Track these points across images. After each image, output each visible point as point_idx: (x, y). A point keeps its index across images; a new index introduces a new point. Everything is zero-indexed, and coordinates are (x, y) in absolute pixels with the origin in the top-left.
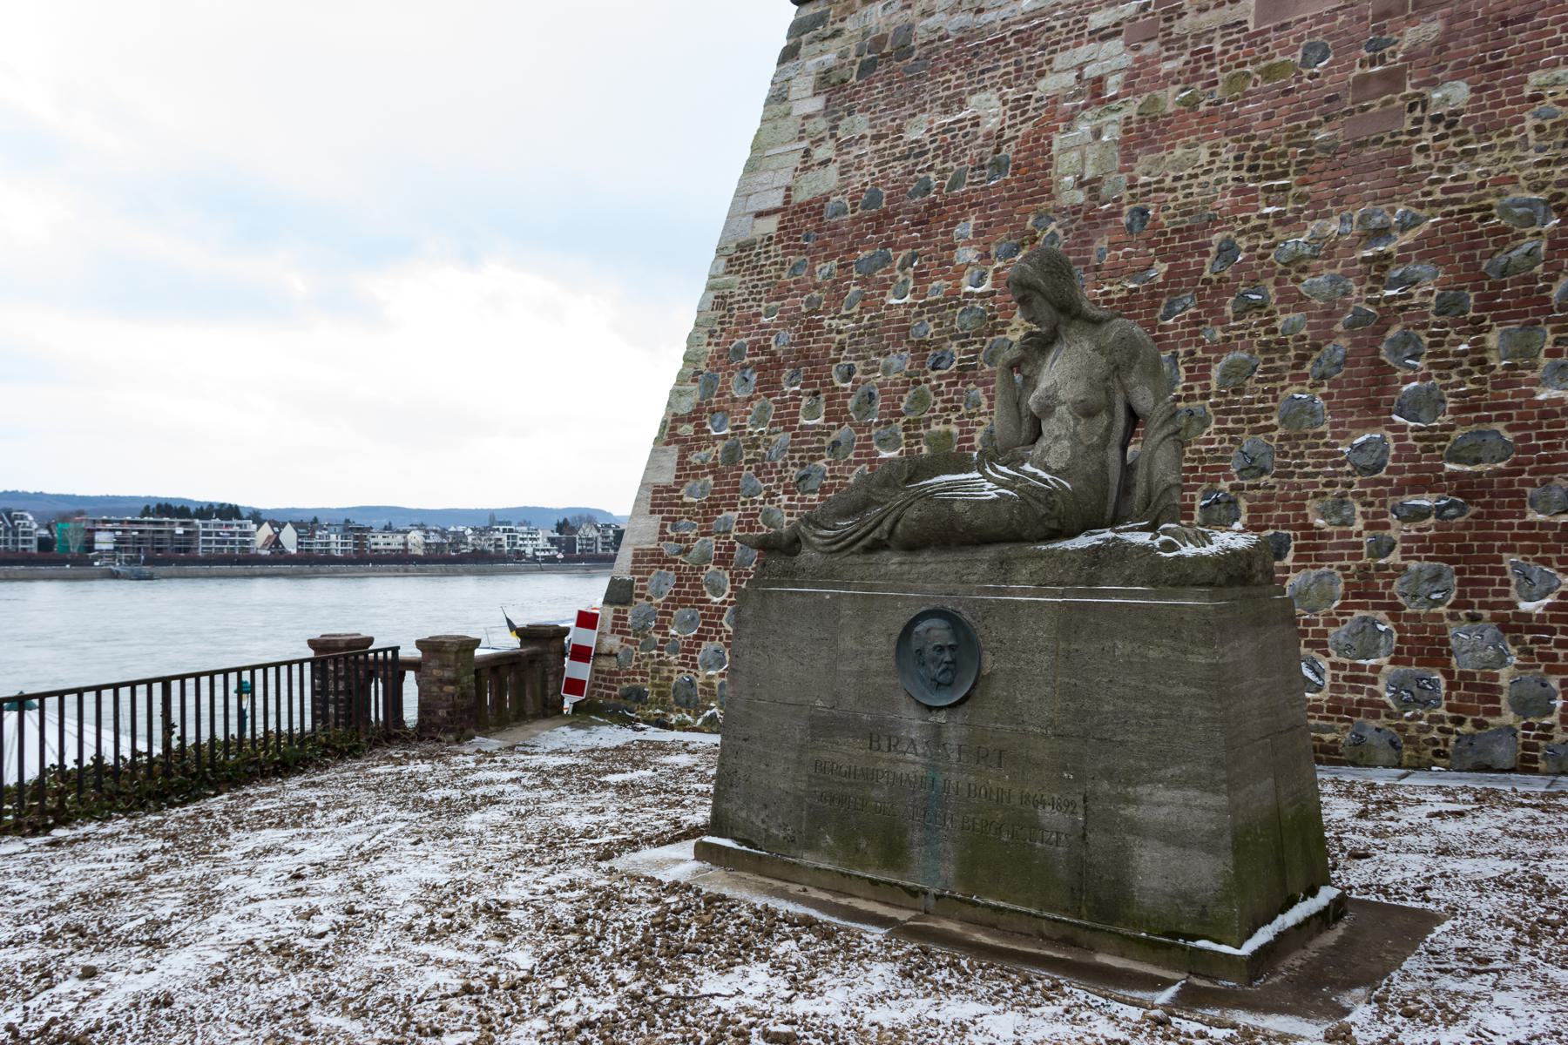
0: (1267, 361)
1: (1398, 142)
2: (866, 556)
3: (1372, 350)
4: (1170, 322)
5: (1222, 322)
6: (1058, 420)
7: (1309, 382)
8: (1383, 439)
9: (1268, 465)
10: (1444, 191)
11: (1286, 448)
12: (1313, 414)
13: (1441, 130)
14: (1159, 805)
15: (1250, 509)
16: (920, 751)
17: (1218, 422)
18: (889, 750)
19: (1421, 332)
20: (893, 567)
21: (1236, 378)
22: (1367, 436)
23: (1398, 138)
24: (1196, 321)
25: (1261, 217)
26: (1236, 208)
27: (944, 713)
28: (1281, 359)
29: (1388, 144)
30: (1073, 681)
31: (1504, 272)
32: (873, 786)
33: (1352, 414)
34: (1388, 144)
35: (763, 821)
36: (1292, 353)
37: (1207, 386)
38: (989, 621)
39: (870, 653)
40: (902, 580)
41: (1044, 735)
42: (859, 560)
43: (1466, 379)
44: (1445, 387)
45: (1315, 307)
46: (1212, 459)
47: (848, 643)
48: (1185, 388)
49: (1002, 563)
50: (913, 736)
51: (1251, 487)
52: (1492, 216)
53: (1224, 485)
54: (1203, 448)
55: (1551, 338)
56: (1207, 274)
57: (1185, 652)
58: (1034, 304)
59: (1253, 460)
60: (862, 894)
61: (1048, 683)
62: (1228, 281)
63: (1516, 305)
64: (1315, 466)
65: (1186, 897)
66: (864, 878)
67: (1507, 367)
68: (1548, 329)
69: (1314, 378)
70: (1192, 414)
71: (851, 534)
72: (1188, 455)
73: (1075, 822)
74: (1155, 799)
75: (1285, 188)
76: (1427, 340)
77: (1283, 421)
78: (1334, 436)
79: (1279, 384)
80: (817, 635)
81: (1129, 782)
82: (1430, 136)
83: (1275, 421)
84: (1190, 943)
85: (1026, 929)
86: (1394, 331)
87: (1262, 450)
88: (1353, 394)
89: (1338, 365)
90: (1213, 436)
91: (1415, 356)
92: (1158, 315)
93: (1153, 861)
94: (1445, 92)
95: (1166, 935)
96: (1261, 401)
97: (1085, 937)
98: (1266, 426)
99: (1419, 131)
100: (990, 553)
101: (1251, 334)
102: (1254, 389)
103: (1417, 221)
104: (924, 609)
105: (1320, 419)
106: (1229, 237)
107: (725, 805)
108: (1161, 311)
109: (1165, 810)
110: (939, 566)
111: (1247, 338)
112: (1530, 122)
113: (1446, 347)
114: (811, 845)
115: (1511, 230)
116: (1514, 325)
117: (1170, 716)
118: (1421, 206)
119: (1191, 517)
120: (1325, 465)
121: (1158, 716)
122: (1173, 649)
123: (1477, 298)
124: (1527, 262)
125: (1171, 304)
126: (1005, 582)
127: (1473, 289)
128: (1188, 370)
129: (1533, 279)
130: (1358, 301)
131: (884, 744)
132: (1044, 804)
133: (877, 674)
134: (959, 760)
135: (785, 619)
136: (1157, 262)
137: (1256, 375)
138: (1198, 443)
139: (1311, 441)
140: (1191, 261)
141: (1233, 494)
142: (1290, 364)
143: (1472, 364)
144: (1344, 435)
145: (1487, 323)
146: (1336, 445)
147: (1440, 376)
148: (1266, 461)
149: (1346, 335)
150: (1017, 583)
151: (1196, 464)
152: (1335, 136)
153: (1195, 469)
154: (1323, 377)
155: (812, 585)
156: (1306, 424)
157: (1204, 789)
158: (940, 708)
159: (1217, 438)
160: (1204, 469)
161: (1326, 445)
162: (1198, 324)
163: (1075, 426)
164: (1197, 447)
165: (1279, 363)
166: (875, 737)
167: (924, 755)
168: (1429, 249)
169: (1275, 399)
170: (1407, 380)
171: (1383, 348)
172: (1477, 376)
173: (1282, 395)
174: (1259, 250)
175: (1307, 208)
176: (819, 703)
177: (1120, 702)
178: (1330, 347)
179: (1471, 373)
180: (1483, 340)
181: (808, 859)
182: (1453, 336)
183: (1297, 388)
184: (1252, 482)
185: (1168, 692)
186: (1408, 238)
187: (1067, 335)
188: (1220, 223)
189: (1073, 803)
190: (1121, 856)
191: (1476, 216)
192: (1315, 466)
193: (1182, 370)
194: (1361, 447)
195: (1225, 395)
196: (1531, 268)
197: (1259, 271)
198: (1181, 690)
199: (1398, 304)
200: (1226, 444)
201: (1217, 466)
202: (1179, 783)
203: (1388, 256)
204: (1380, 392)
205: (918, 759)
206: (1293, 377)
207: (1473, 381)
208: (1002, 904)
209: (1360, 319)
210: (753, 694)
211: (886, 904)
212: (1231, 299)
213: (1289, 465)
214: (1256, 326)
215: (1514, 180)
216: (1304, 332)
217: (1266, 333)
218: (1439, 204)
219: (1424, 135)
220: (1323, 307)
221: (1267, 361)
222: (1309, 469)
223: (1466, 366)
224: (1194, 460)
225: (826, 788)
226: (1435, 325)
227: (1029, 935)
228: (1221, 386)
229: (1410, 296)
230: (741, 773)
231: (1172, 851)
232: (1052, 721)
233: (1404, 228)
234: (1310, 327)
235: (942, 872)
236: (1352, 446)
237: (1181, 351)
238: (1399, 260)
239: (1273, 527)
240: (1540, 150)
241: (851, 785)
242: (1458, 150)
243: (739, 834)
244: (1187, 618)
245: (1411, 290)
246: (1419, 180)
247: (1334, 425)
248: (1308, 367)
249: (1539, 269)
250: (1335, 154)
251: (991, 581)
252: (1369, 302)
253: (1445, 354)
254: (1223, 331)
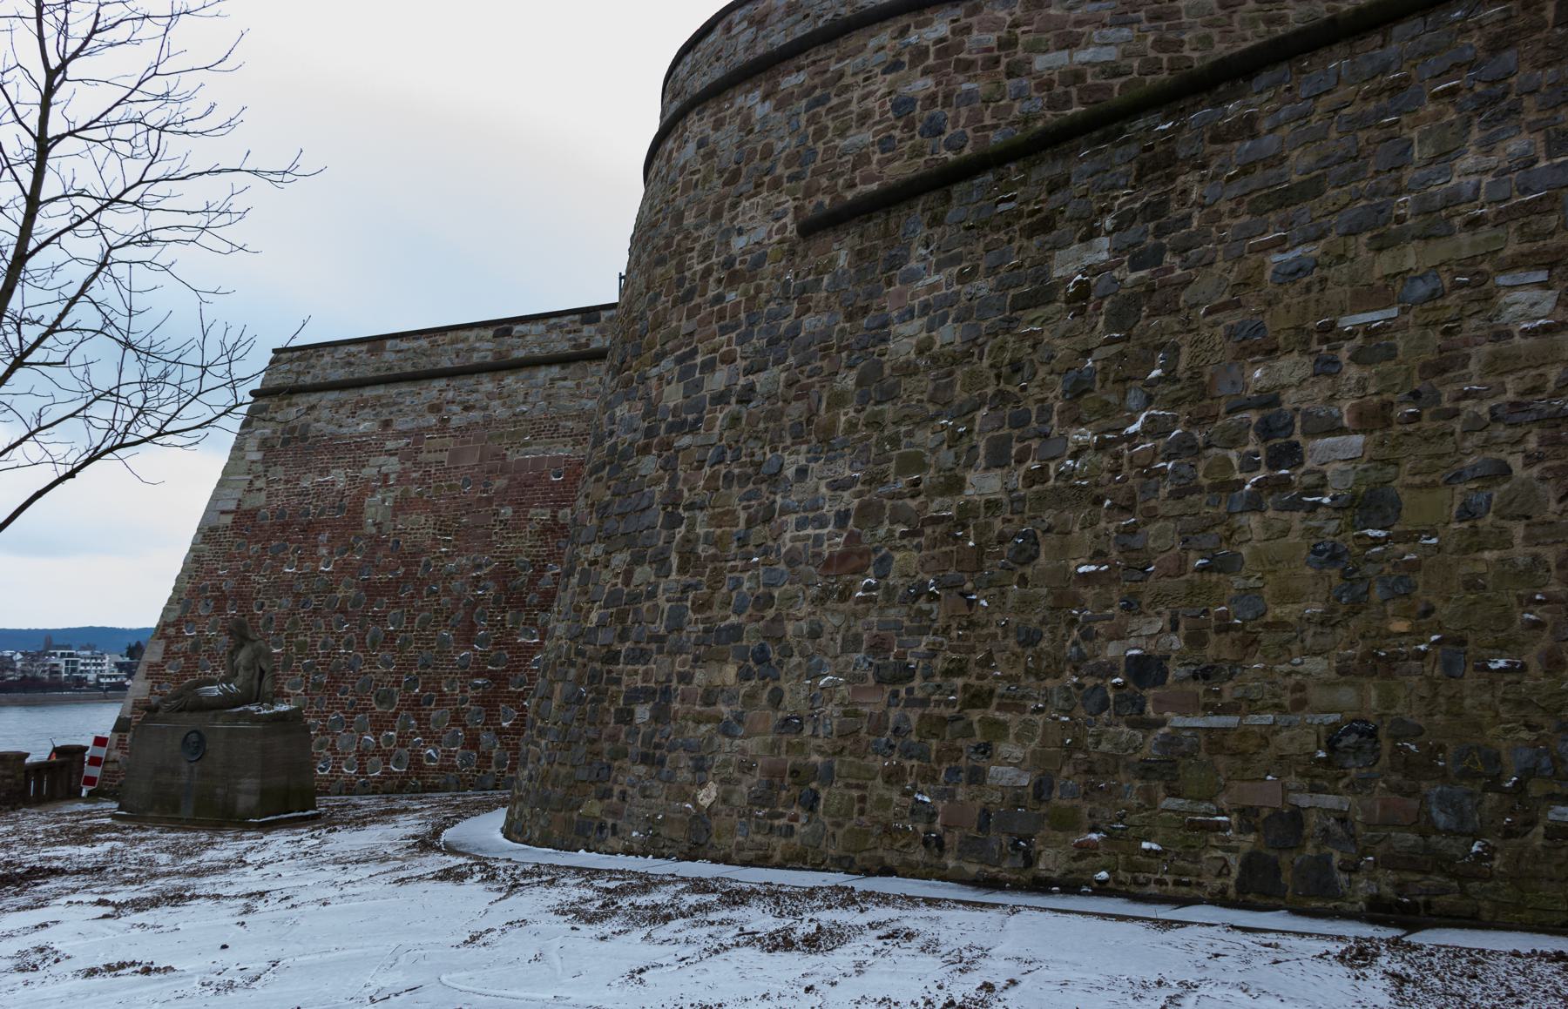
5: (422, 598)
100: (212, 713)
112: (528, 529)
148: (430, 662)
181: (150, 814)
186: (486, 570)
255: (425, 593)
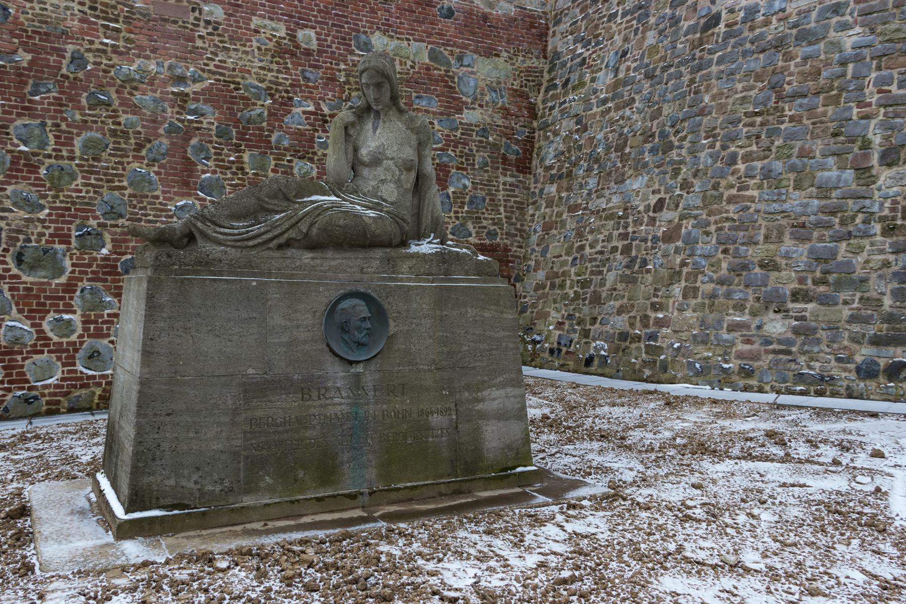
0: (115, 142)
1: (187, 28)
2: (282, 252)
3: (183, 150)
4: (37, 98)
5: (81, 109)
6: (385, 169)
7: (146, 162)
8: (194, 204)
9: (123, 213)
10: (215, 66)
11: (135, 202)
12: (150, 183)
13: (210, 30)
14: (494, 400)
15: (113, 240)
16: (344, 394)
17: (83, 178)
18: (319, 398)
19: (209, 145)
20: (307, 261)
21: (94, 149)
22: (184, 202)
23: (186, 25)
24: (58, 102)
25: (102, 43)
26: (82, 32)
27: (362, 365)
28: (125, 143)
29: (180, 26)
30: (445, 334)
31: (248, 122)
32: (306, 428)
33: (174, 187)
34: (180, 26)
35: (196, 483)
36: (133, 141)
37: (72, 151)
38: (390, 299)
39: (298, 327)
40: (316, 271)
41: (430, 370)
42: (277, 254)
43: (235, 177)
44: (225, 179)
45: (145, 114)
46: (81, 204)
47: (276, 319)
48: (54, 150)
49: (389, 260)
50: (338, 385)
51: (112, 226)
52: (240, 89)
53: (93, 223)
54: (74, 195)
55: (273, 163)
56: (64, 71)
57: (502, 312)
58: (384, 89)
59: (112, 207)
60: (310, 511)
61: (430, 337)
62: (81, 80)
63: (257, 141)
64: (154, 216)
65: (509, 447)
66: (311, 499)
67: (254, 174)
68: (272, 157)
69: (149, 160)
70: (62, 169)
71: (264, 233)
72: (62, 198)
73: (451, 420)
74: (492, 397)
75: (118, 30)
76: (213, 151)
77: (131, 184)
78: (165, 198)
79: (125, 160)
80: (244, 315)
81: (479, 390)
82: (205, 31)
83: (125, 183)
84: (513, 471)
85: (432, 494)
86: (194, 141)
87: (118, 202)
88: (174, 175)
89: (163, 154)
90: (80, 187)
91: (207, 159)
92: (26, 91)
93: (493, 431)
94: (212, 8)
95: (502, 470)
96: (113, 169)
97: (465, 486)
98: (119, 186)
99: (198, 26)
100: (379, 253)
101: (102, 122)
102: (107, 161)
103: (201, 80)
104: (342, 292)
105: (155, 187)
106: (79, 50)
107: (146, 480)
108: (28, 88)
109: (497, 402)
110: (344, 261)
111: (100, 124)
112: (255, 44)
113: (223, 157)
114: (250, 488)
115: (250, 100)
116: (256, 152)
117: (497, 349)
118: (203, 70)
119: (69, 243)
120: (161, 216)
121: (491, 350)
122: (496, 311)
123: (237, 133)
124: (259, 120)
125: (36, 85)
126: (394, 273)
127: (235, 127)
128: (56, 137)
129: (261, 129)
130: (171, 117)
131: (315, 394)
132: (432, 413)
133: (305, 342)
134: (375, 395)
135: (209, 303)
136: (20, 50)
137: (108, 150)
138: (69, 190)
139: (149, 199)
140: (52, 58)
141: (99, 229)
142: (132, 148)
143: (237, 169)
144: (171, 199)
145: (243, 147)
146: (166, 205)
147: (221, 173)
148: (122, 209)
149: (167, 137)
150: (402, 273)
151: (69, 205)
152: (148, 9)
153: (69, 209)
154: (154, 160)
155: (231, 273)
156: (146, 189)
157: (514, 386)
158: (358, 362)
159: (84, 189)
160: (75, 209)
161: (160, 203)
162: (61, 105)
163: (400, 175)
164: (69, 193)
165: (123, 146)
166: (305, 390)
167: (349, 397)
168: (208, 96)
169: (124, 169)
170: (204, 172)
171: (189, 150)
172: (240, 176)
173: (128, 167)
174: (103, 66)
175: (133, 48)
176: (251, 371)
177: (472, 344)
178: (157, 142)
179: (237, 174)
180: (241, 157)
181: (248, 501)
182: (226, 151)
183: (138, 165)
184: (113, 222)
185: (496, 336)
186: (197, 87)
187: (386, 115)
188: (72, 38)
189: (450, 409)
190: (477, 433)
191: (232, 86)
192: (154, 216)
193: (51, 136)
194: (182, 208)
195: (87, 160)
196: (261, 123)
197: (104, 81)
198: (502, 334)
199: (195, 125)
200: (91, 194)
201: (86, 210)
202: (502, 385)
203: (187, 95)
204: (189, 176)
205: (343, 401)
206: (134, 157)
207: (238, 179)
208: (415, 484)
209: (172, 130)
210: (176, 373)
211: (332, 511)
212: (85, 94)
213: (138, 214)
214: (105, 117)
215: (249, 72)
216: (139, 129)
217: (114, 123)
218: (214, 73)
219: (201, 29)
220: (150, 116)
221: (115, 142)
222: (151, 218)
223: (234, 170)
224: (68, 203)
225: (264, 439)
226: (216, 143)
227: (434, 497)
228: (83, 153)
229: (201, 122)
230: (165, 446)
231: (501, 424)
232: (434, 360)
233: (195, 81)
234: (143, 126)
235: (367, 476)
236: (176, 207)
237: (49, 122)
238: (194, 99)
239: (130, 253)
240: (261, 61)
241: (287, 431)
242: (221, 45)
243: (168, 501)
244: (502, 293)
245: (201, 119)
246: (201, 55)
247: (164, 192)
248: (144, 152)
249: (265, 124)
250: (149, 20)
251: (384, 272)
252: (177, 119)
253: (223, 161)
254: (81, 114)
255: (84, 101)
